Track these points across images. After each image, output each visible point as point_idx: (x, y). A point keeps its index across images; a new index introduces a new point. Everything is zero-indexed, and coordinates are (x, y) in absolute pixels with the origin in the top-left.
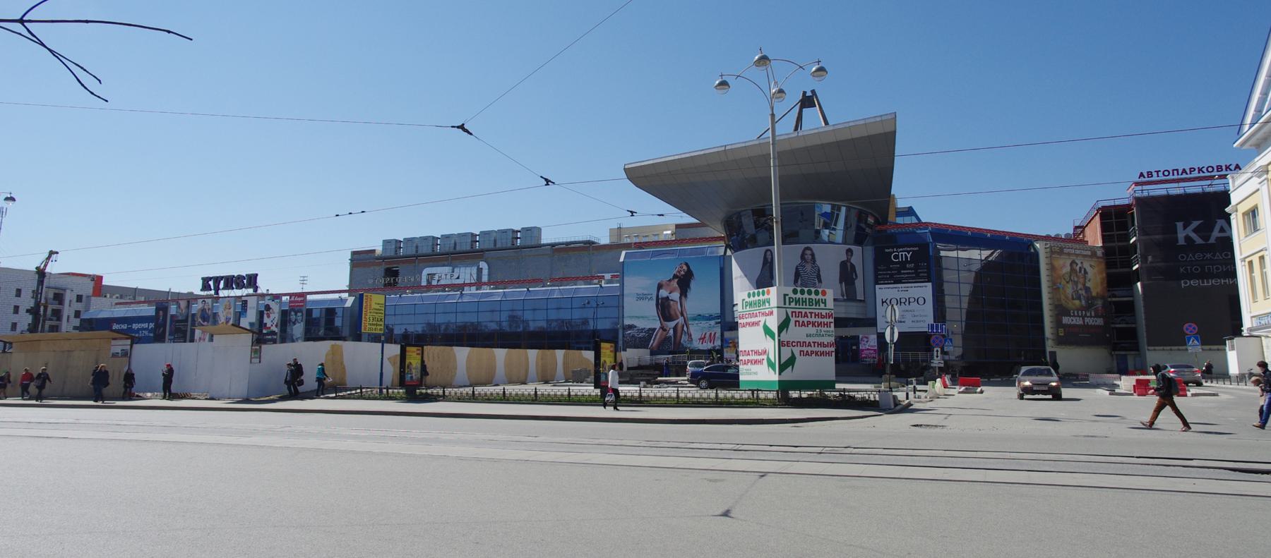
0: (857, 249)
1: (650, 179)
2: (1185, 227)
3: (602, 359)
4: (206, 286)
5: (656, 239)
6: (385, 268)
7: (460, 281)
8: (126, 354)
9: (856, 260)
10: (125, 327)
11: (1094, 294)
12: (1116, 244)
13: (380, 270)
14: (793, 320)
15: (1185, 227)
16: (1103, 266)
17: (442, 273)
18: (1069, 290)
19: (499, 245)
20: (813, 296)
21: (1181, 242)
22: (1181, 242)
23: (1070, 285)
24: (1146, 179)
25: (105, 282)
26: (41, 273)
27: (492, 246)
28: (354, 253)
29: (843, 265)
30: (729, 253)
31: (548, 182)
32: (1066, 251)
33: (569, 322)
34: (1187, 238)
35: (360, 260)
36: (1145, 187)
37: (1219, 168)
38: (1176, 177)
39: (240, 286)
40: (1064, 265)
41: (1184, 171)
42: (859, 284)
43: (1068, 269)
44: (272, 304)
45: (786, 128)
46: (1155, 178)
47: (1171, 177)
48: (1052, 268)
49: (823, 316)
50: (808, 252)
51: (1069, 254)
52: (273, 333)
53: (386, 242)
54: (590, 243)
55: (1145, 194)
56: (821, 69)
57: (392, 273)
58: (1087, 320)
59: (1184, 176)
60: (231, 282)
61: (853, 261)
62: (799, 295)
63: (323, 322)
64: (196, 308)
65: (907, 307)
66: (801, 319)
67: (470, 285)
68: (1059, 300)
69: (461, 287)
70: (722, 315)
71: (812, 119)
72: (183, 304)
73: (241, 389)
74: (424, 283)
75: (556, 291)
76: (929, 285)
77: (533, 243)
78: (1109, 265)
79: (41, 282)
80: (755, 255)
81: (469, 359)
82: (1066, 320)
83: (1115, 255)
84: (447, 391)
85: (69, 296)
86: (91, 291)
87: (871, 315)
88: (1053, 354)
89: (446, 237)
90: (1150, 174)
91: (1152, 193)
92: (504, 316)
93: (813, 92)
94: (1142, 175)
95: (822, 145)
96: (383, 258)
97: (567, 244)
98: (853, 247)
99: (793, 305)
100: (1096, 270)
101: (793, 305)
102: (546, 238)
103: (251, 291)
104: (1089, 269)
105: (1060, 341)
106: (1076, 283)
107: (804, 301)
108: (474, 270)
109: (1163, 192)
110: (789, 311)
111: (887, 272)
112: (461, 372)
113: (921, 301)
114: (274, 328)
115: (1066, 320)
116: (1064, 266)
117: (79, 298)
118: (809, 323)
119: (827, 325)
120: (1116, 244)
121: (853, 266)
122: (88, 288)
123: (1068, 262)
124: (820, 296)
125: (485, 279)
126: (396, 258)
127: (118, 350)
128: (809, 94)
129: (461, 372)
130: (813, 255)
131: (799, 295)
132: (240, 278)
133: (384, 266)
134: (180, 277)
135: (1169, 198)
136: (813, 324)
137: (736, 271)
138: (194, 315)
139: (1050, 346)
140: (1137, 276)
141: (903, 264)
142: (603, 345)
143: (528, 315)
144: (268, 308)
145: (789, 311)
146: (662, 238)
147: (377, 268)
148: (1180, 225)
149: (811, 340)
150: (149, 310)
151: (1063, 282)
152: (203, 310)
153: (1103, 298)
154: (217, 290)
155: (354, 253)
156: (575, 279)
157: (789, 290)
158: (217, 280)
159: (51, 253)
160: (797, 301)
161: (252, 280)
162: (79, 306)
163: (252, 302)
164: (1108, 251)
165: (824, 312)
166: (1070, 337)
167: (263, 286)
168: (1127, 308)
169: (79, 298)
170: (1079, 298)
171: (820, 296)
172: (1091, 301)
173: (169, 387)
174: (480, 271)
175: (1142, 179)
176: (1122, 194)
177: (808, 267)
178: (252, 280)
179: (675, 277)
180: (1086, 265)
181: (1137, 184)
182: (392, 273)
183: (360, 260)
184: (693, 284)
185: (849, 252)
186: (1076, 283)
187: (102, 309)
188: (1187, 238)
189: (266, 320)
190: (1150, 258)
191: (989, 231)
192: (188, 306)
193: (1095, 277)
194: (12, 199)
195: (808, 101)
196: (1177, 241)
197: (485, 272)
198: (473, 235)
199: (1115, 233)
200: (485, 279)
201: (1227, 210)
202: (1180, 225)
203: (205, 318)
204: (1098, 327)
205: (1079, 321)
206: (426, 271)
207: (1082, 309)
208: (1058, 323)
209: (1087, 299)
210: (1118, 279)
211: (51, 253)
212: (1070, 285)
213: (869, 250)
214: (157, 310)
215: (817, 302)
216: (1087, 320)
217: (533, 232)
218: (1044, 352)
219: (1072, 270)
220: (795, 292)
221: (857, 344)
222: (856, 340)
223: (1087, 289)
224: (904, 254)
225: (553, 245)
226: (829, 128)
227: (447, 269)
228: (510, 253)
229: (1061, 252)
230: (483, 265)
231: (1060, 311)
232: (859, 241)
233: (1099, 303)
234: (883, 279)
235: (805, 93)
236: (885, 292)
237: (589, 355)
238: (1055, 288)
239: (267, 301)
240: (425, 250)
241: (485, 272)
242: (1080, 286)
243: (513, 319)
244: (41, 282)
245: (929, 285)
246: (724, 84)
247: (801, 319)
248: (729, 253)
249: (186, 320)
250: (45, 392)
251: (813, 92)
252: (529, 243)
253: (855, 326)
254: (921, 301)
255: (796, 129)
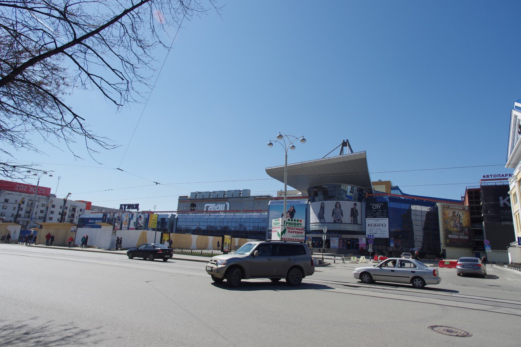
0: (359, 204)
1: (275, 173)
2: (503, 199)
3: (225, 241)
4: (121, 208)
5: (295, 196)
6: (191, 203)
7: (218, 210)
8: (75, 231)
9: (358, 208)
10: (93, 221)
11: (464, 226)
12: (474, 205)
13: (189, 204)
14: (287, 230)
15: (503, 199)
16: (468, 214)
17: (212, 207)
18: (452, 223)
19: (234, 196)
20: (296, 222)
21: (502, 205)
22: (502, 205)
23: (452, 222)
24: (486, 178)
25: (92, 205)
26: (65, 201)
27: (231, 196)
28: (180, 197)
29: (352, 210)
30: (309, 203)
31: (157, 183)
32: (450, 207)
33: (213, 227)
34: (504, 204)
35: (182, 200)
36: (502, 181)
37: (506, 175)
38: (499, 178)
39: (133, 208)
40: (449, 213)
41: (503, 175)
42: (359, 218)
43: (451, 215)
44: (142, 216)
45: (336, 154)
46: (490, 178)
47: (497, 178)
48: (444, 214)
49: (299, 230)
50: (338, 204)
51: (452, 208)
52: (141, 226)
53: (192, 193)
54: (269, 196)
55: (486, 184)
56: (304, 139)
57: (193, 205)
58: (460, 237)
59: (503, 177)
60: (130, 206)
61: (357, 208)
62: (290, 221)
63: (165, 225)
64: (116, 216)
65: (378, 228)
66: (291, 230)
67: (222, 211)
68: (447, 227)
69: (219, 212)
70: (306, 228)
71: (346, 149)
72: (112, 214)
73: (108, 245)
74: (205, 210)
75: (244, 215)
76: (387, 219)
77: (247, 196)
78: (472, 213)
79: (65, 204)
80: (318, 204)
81: (197, 239)
82: (450, 236)
83: (474, 211)
84: (183, 250)
85: (77, 209)
86: (85, 208)
87: (364, 230)
88: (444, 251)
89: (229, 191)
90: (488, 176)
91: (489, 184)
92: (237, 225)
93: (347, 140)
94: (484, 176)
95: (356, 160)
96: (190, 199)
97: (260, 196)
98: (356, 203)
99: (288, 225)
100: (465, 216)
101: (288, 225)
102: (252, 194)
103: (136, 210)
104: (461, 215)
105: (447, 245)
106: (455, 221)
107: (292, 224)
108: (224, 205)
109: (494, 184)
110: (286, 227)
111: (370, 213)
112: (194, 244)
113: (384, 225)
114: (142, 225)
115: (450, 236)
116: (450, 213)
117: (81, 210)
118: (294, 232)
119: (302, 233)
120: (474, 205)
121: (356, 210)
122: (84, 206)
123: (451, 212)
124: (299, 222)
125: (228, 209)
126: (196, 200)
127: (72, 229)
128: (346, 141)
129: (194, 244)
130: (340, 205)
131: (290, 221)
132: (133, 205)
133: (191, 203)
134: (113, 203)
135: (496, 186)
136: (296, 232)
137: (311, 211)
138: (115, 218)
139: (443, 247)
140: (481, 220)
141: (377, 210)
142: (225, 236)
143: (246, 225)
144: (140, 217)
145: (286, 227)
146: (297, 196)
147: (188, 203)
148: (501, 198)
149: (294, 238)
150: (101, 216)
151: (449, 220)
152: (119, 217)
153: (468, 227)
154: (125, 209)
155: (180, 197)
156: (253, 211)
157: (287, 220)
158: (125, 205)
159: (69, 194)
160: (289, 224)
161: (137, 206)
162: (80, 213)
163: (135, 215)
164: (471, 208)
165: (300, 228)
166: (452, 243)
167: (141, 209)
168: (479, 233)
169: (81, 210)
170: (457, 227)
171: (299, 222)
172: (462, 229)
173: (85, 243)
174: (226, 206)
175: (484, 178)
176: (477, 185)
177: (338, 210)
178: (137, 206)
179: (289, 211)
180: (460, 213)
181: (482, 180)
182: (193, 205)
183: (182, 200)
184: (295, 215)
185: (355, 204)
186: (455, 221)
187: (88, 214)
188: (504, 204)
189: (139, 221)
190: (489, 212)
191: (424, 197)
192: (114, 215)
193: (464, 219)
194: (51, 176)
195: (345, 144)
196: (500, 204)
197: (228, 206)
198: (224, 192)
199: (474, 200)
200: (228, 209)
201: (509, 193)
202: (501, 198)
203: (119, 219)
204: (466, 240)
205: (457, 237)
206: (206, 205)
207: (458, 232)
208: (446, 237)
209: (461, 228)
210: (475, 220)
211: (69, 194)
212: (452, 222)
213: (364, 204)
214: (103, 216)
215: (298, 224)
216: (460, 237)
217: (247, 191)
218: (440, 249)
219: (454, 215)
220: (289, 220)
221: (358, 242)
222: (357, 240)
223: (461, 224)
224: (378, 206)
225: (254, 197)
226: (353, 154)
227: (214, 205)
228: (238, 199)
229: (448, 207)
230: (228, 204)
231: (447, 232)
232: (360, 200)
233: (467, 230)
234: (369, 216)
235: (344, 141)
236: (369, 221)
237: (220, 239)
238: (445, 222)
239: (140, 214)
240: (206, 197)
241: (228, 206)
242: (457, 222)
243: (241, 225)
244: (65, 204)
245: (387, 219)
246: (271, 144)
247: (291, 230)
248: (309, 203)
249: (112, 220)
250: (54, 242)
251: (347, 140)
252: (245, 196)
253: (352, 234)
254: (384, 225)
255: (341, 154)
